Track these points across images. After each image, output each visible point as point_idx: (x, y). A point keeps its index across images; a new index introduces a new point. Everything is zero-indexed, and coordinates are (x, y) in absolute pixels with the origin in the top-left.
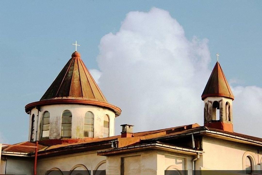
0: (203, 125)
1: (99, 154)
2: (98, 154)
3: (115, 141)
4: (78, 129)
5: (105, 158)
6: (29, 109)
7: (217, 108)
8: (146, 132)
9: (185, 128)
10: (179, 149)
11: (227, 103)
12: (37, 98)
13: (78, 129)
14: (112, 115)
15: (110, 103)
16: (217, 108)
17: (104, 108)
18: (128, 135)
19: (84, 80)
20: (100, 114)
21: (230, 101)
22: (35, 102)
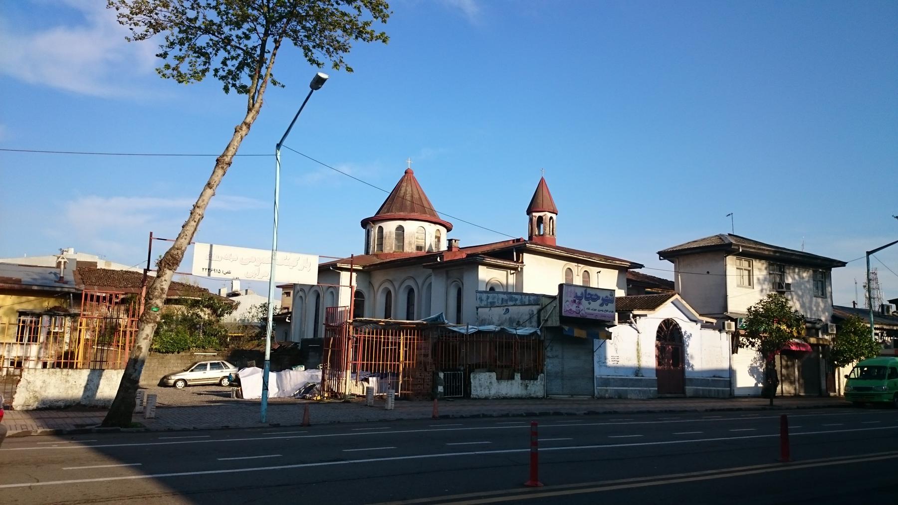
0: (315, 283)
1: (424, 267)
2: (311, 300)
3: (441, 254)
4: (410, 244)
5: (431, 271)
6: (365, 223)
7: (299, 348)
8: (34, 269)
9: (209, 366)
10: (500, 262)
11: (551, 218)
12: (372, 214)
13: (410, 244)
14: (443, 230)
15: (443, 218)
16: (299, 348)
17: (435, 223)
18: (454, 250)
19: (415, 192)
20: (431, 229)
21: (554, 216)
22: (726, 296)
